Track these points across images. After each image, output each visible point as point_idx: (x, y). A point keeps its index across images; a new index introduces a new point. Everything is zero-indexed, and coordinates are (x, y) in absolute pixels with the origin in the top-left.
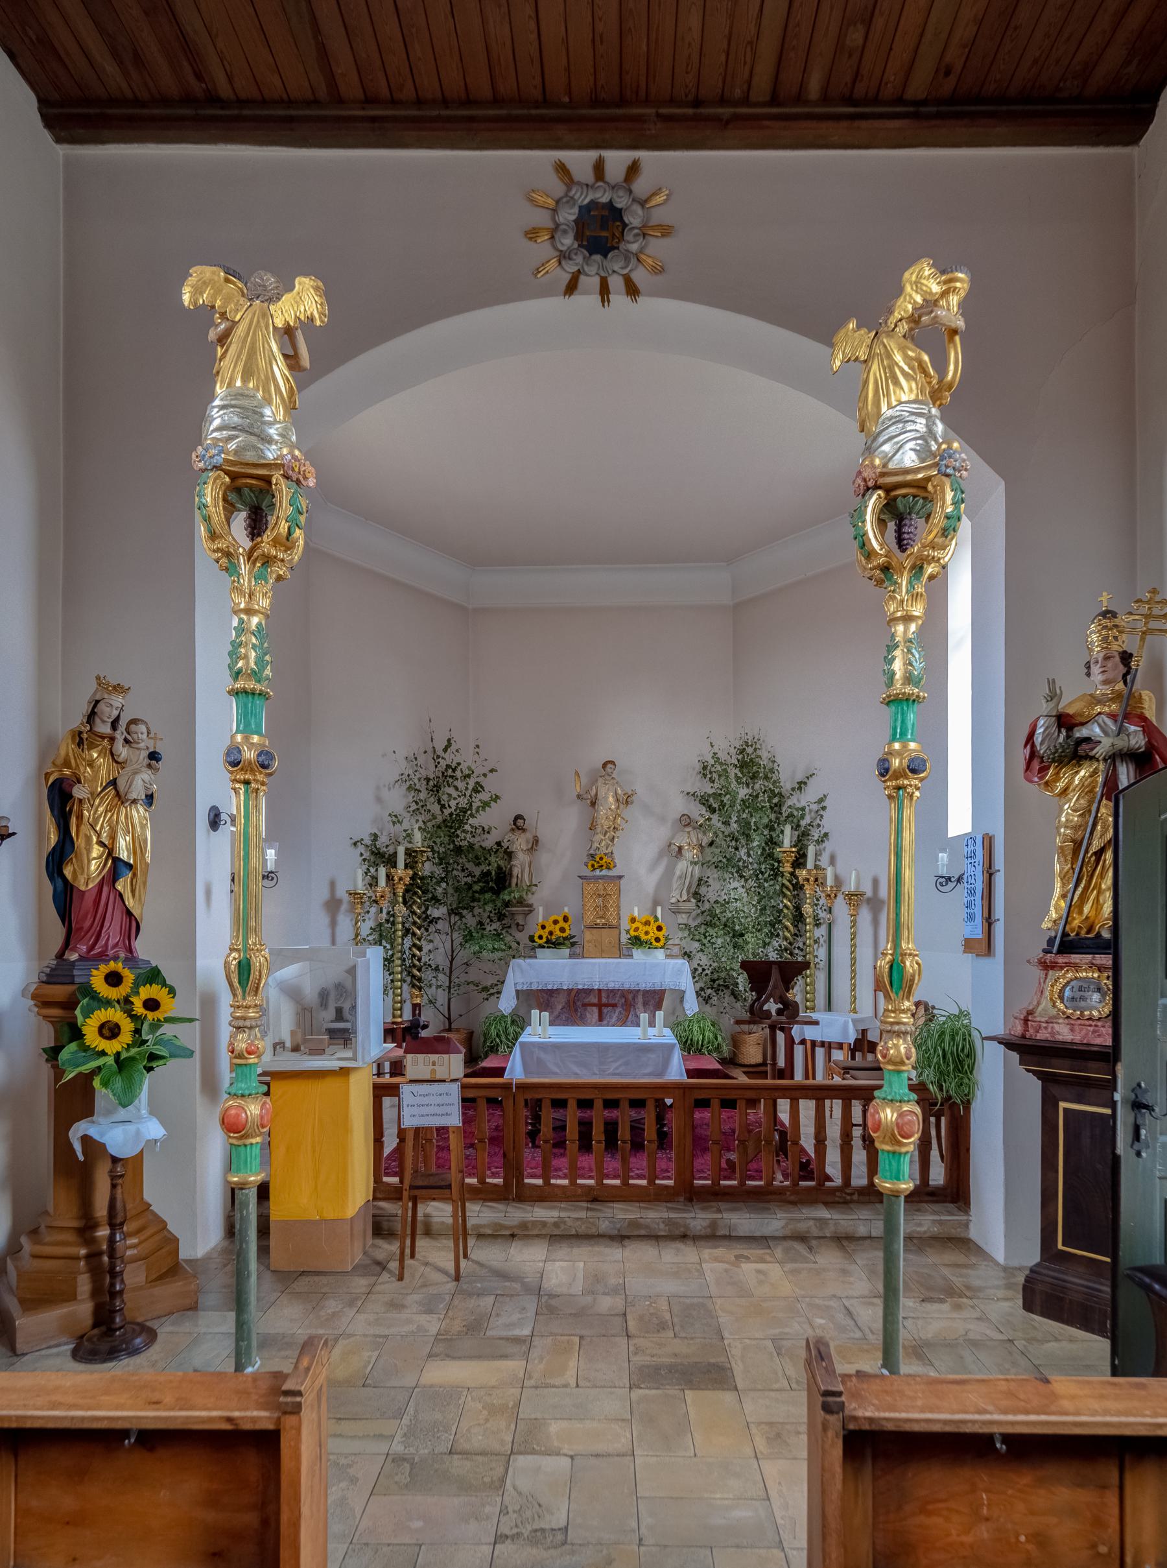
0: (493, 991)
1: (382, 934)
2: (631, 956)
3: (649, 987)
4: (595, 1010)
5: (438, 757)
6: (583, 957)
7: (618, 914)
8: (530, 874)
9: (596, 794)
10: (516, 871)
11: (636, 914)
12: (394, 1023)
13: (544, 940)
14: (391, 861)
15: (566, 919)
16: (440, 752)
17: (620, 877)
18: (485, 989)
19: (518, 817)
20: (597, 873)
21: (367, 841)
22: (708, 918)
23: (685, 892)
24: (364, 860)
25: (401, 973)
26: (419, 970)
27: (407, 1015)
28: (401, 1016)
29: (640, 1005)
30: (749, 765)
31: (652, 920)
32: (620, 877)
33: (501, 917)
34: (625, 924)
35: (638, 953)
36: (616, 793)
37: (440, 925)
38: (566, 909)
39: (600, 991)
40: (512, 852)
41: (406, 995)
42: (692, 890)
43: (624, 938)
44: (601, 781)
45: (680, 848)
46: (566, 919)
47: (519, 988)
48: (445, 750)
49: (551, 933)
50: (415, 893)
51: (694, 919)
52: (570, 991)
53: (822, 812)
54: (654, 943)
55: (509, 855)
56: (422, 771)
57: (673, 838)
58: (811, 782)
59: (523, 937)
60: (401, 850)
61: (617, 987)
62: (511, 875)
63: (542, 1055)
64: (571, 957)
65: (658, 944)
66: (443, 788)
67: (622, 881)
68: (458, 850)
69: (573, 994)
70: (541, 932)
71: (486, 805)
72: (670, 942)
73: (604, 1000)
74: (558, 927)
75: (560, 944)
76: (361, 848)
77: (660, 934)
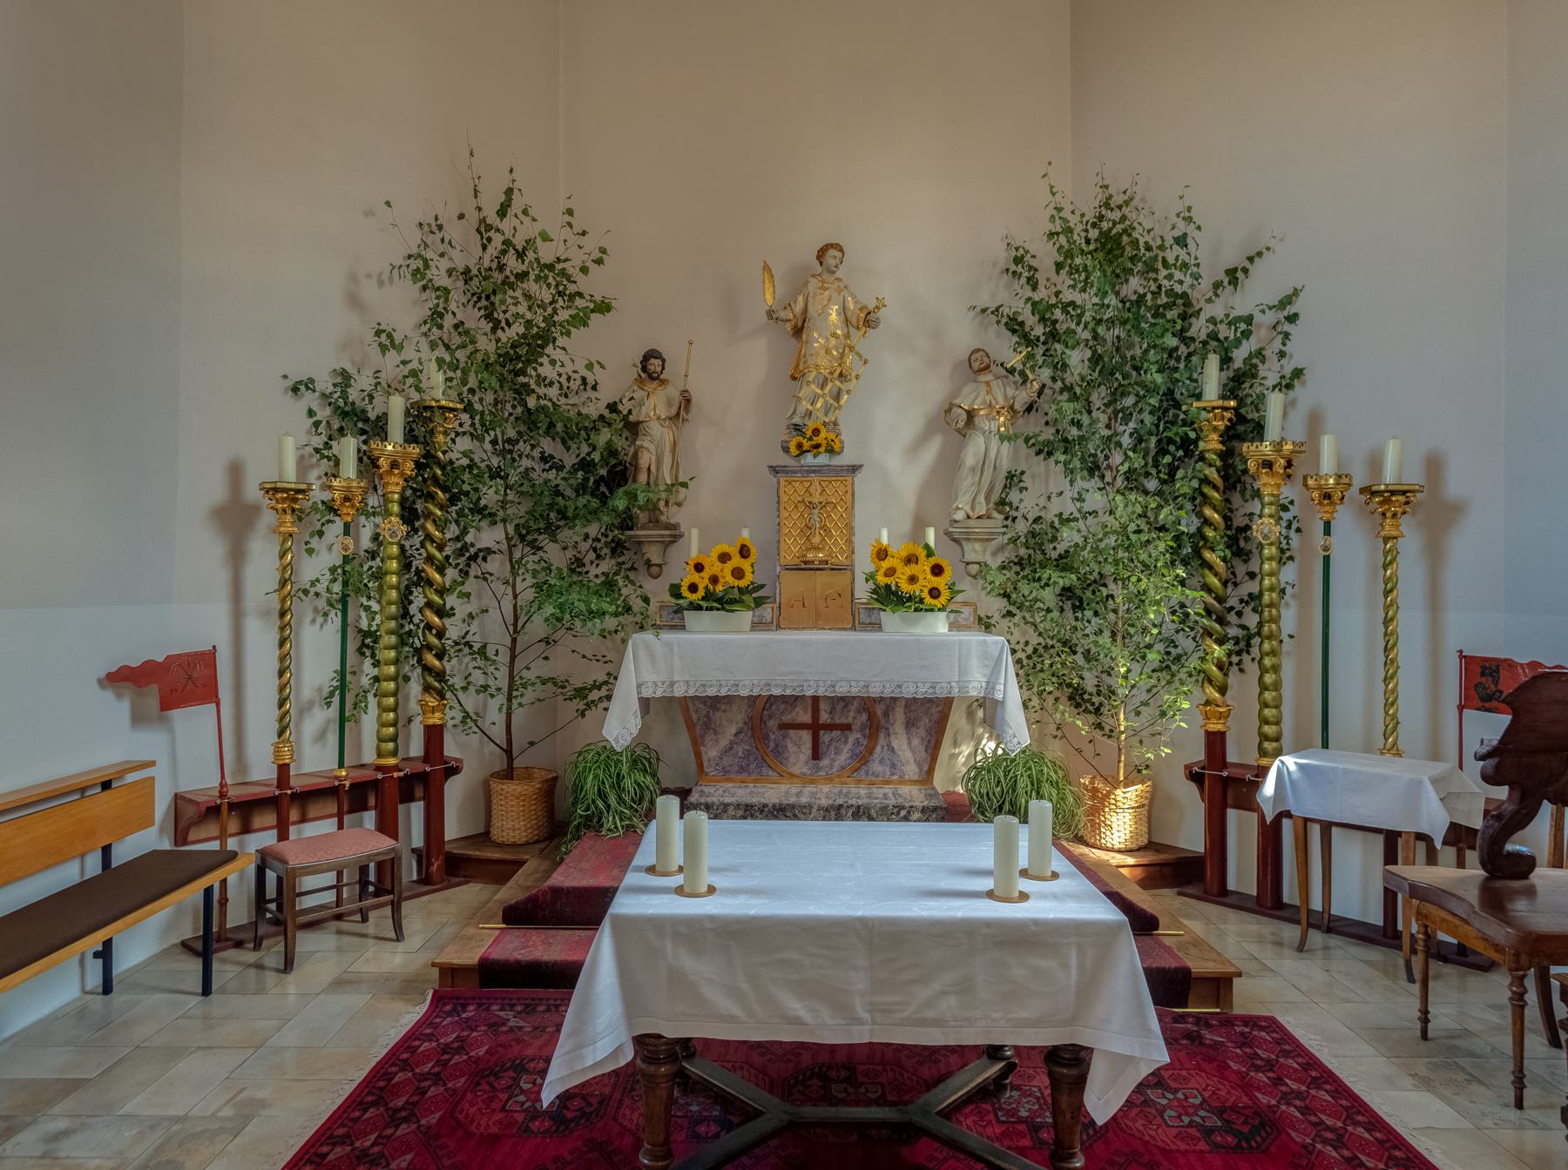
0: (592, 696)
1: (351, 581)
2: (877, 626)
3: (923, 691)
4: (806, 736)
5: (489, 228)
6: (779, 627)
7: (850, 542)
8: (675, 465)
9: (805, 311)
10: (645, 460)
11: (885, 540)
12: (379, 768)
13: (701, 593)
14: (379, 428)
15: (744, 552)
16: (492, 219)
17: (854, 469)
18: (581, 693)
19: (650, 355)
20: (809, 459)
21: (325, 383)
22: (1023, 552)
23: (981, 498)
24: (317, 424)
25: (396, 662)
26: (440, 657)
27: (416, 748)
28: (394, 753)
29: (898, 726)
30: (1111, 246)
31: (922, 554)
32: (854, 469)
33: (617, 548)
34: (864, 563)
35: (891, 620)
36: (844, 308)
37: (495, 565)
38: (745, 533)
39: (816, 700)
40: (638, 423)
41: (414, 707)
42: (995, 497)
43: (863, 591)
44: (813, 284)
45: (971, 415)
46: (744, 552)
47: (647, 693)
48: (502, 213)
49: (714, 580)
50: (431, 497)
51: (994, 554)
52: (752, 699)
53: (1287, 327)
54: (928, 600)
55: (633, 428)
56: (455, 254)
57: (956, 392)
58: (1257, 269)
59: (657, 590)
60: (396, 408)
61: (855, 691)
62: (637, 468)
63: (687, 961)
64: (757, 626)
65: (937, 603)
66: (504, 298)
67: (859, 478)
68: (530, 420)
69: (760, 704)
70: (695, 577)
71: (581, 320)
72: (959, 598)
73: (824, 717)
74: (729, 566)
75: (733, 601)
76: (310, 400)
77: (940, 582)
